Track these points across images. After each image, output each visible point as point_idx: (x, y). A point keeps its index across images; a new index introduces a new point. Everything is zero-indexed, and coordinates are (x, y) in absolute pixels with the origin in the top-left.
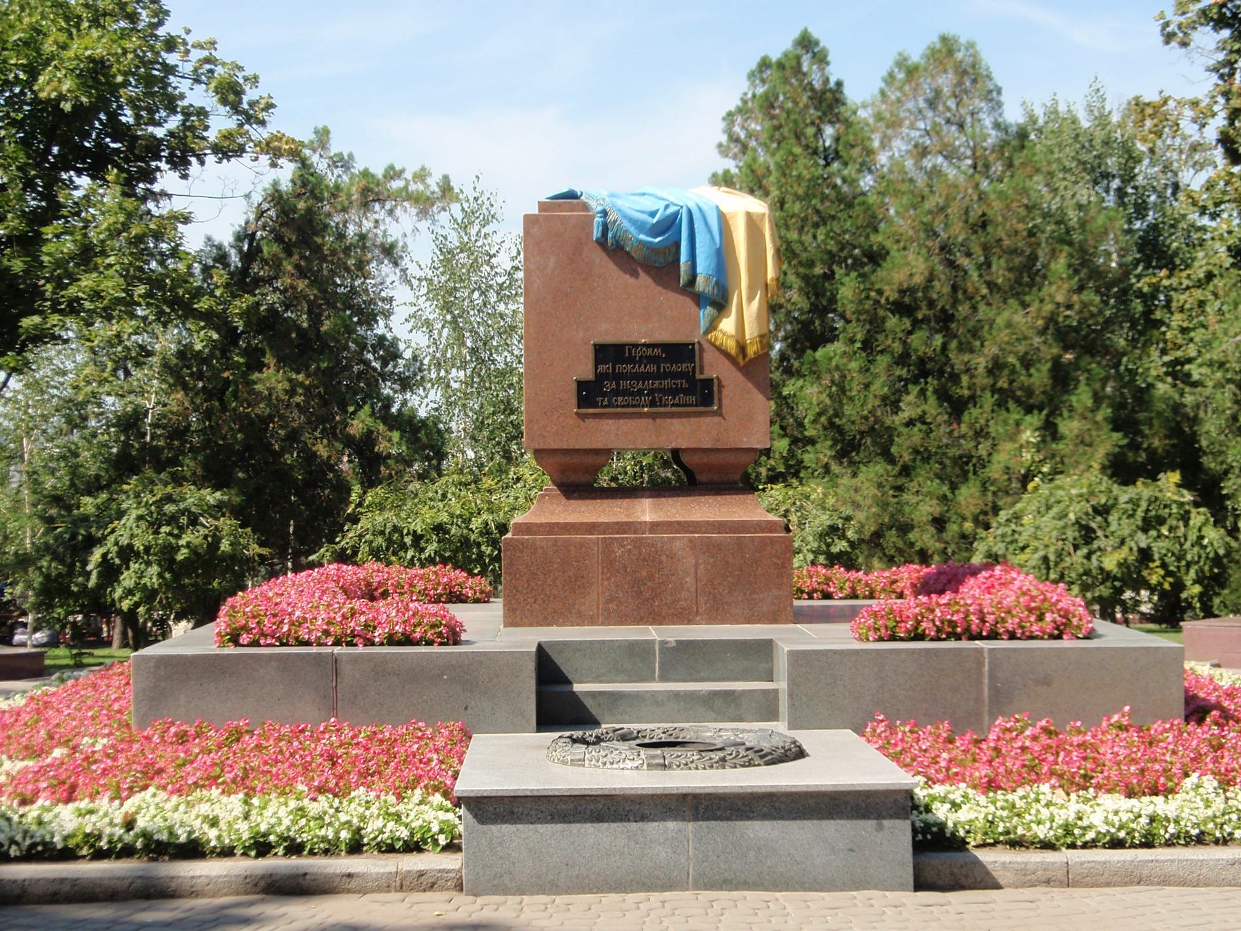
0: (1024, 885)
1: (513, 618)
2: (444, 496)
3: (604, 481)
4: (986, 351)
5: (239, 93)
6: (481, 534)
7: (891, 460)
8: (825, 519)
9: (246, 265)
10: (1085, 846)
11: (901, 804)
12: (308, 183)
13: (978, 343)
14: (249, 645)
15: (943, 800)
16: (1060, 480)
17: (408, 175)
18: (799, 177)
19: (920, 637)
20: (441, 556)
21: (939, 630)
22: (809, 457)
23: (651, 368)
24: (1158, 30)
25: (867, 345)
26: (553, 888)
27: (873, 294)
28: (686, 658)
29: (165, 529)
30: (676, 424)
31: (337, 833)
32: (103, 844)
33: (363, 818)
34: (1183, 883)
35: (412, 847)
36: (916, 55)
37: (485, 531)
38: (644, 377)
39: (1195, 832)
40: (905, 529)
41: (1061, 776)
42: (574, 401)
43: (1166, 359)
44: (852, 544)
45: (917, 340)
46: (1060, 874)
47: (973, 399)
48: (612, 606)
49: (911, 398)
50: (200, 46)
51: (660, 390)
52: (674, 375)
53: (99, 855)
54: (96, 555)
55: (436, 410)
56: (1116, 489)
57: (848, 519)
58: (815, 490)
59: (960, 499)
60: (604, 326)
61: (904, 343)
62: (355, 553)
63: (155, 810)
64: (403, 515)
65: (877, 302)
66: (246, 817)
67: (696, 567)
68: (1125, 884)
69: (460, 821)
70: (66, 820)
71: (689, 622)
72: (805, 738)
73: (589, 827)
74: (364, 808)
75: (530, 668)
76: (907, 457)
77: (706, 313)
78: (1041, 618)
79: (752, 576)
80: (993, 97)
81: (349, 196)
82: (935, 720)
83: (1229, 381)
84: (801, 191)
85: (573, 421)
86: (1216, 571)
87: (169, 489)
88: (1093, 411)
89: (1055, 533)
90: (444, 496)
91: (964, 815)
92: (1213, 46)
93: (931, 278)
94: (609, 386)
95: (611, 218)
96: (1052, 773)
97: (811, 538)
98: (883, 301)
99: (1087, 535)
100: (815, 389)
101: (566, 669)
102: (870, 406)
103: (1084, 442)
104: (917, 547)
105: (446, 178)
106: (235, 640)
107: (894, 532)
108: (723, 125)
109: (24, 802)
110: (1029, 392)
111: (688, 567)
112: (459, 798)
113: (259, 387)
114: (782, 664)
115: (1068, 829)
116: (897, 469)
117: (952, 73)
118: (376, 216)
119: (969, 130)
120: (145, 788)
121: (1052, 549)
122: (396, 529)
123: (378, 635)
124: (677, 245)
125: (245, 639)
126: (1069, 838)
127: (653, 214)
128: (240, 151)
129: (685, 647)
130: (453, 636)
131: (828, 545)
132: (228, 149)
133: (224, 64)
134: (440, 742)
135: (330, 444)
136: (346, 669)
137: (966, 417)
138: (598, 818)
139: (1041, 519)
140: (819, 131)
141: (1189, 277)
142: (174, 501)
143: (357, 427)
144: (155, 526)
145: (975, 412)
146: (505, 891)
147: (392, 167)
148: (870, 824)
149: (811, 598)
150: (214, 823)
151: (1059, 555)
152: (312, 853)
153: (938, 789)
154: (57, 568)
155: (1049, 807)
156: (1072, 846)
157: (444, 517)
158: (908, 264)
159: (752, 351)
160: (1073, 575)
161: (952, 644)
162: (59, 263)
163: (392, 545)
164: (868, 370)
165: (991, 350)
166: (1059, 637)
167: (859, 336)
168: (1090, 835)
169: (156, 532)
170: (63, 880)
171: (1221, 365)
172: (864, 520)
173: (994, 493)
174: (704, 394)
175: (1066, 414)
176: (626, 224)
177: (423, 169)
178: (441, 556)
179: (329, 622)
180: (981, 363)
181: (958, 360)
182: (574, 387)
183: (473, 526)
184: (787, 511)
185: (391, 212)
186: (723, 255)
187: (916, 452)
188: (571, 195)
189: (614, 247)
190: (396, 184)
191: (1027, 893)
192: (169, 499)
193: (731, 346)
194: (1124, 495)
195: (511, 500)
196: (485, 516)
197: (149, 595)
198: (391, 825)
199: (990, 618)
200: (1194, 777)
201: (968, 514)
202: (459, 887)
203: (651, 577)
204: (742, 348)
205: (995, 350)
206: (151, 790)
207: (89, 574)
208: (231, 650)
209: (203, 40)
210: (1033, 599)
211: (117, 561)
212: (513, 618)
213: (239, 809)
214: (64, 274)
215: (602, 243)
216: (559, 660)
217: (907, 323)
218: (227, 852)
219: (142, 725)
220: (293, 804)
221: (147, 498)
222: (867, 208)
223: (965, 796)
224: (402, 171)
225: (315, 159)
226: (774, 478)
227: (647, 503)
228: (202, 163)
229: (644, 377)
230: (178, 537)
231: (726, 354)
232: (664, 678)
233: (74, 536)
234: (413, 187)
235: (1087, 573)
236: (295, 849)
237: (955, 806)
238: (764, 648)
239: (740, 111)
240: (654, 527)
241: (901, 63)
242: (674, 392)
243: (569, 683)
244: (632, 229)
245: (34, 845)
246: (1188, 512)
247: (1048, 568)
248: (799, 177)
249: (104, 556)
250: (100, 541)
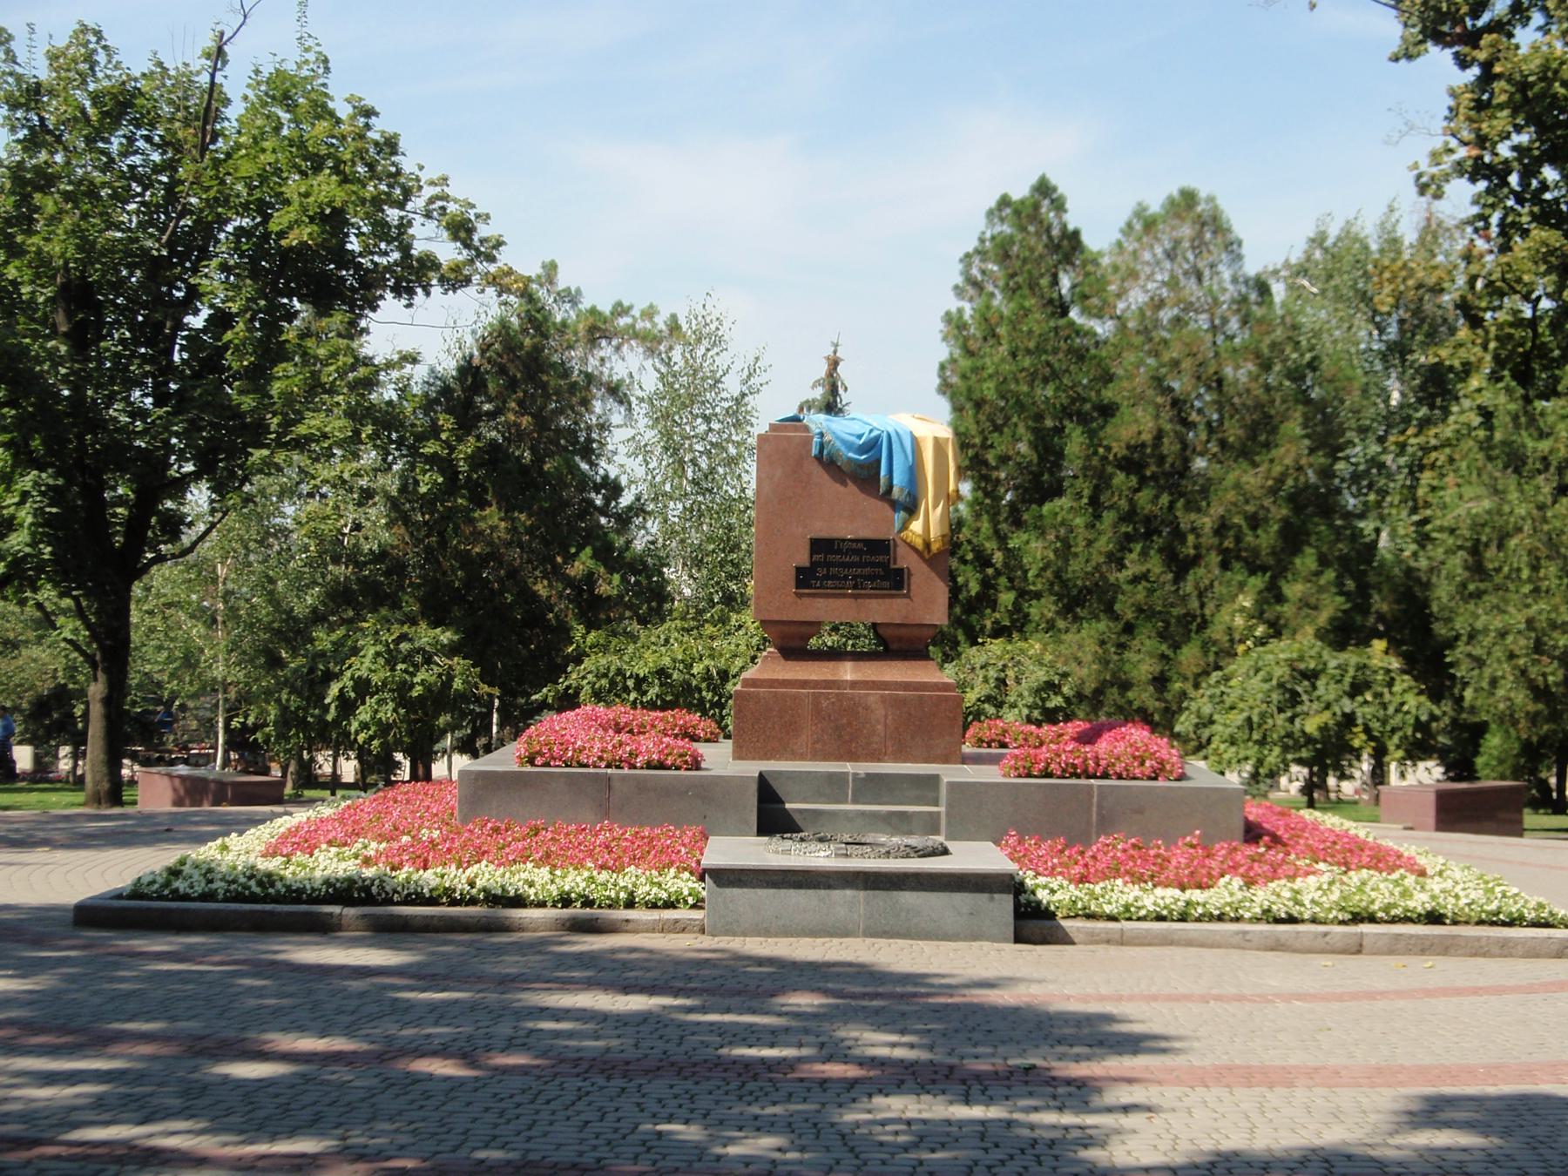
0: (1091, 943)
1: (739, 754)
2: (667, 641)
4: (1212, 511)
5: (470, 231)
6: (704, 679)
7: (1115, 617)
8: (1041, 675)
9: (462, 394)
10: (1139, 919)
12: (536, 319)
13: (1204, 504)
14: (543, 765)
15: (1045, 887)
16: (1274, 644)
17: (636, 312)
18: (1030, 332)
19: (1049, 775)
20: (663, 700)
21: (1064, 770)
22: (1034, 610)
23: (856, 559)
24: (1412, 181)
25: (1094, 501)
27: (1101, 450)
28: (874, 787)
29: (400, 666)
31: (618, 894)
32: (457, 895)
33: (634, 885)
34: (1202, 945)
35: (670, 905)
36: (1155, 206)
37: (707, 676)
39: (1216, 912)
40: (1125, 686)
41: (1132, 875)
42: (793, 583)
43: (1415, 518)
44: (1067, 700)
45: (1144, 497)
46: (1117, 937)
47: (1195, 561)
48: (818, 746)
49: (1134, 556)
50: (432, 183)
51: (861, 576)
52: (873, 565)
53: (454, 902)
54: (334, 689)
55: (653, 543)
56: (1326, 654)
57: (1065, 675)
58: (1032, 646)
59: (1182, 658)
61: (1131, 501)
62: (577, 694)
63: (487, 875)
64: (626, 658)
65: (1104, 458)
66: (552, 882)
67: (886, 717)
69: (704, 889)
70: (429, 878)
71: (879, 760)
72: (950, 845)
73: (792, 892)
74: (637, 879)
75: (754, 787)
76: (1130, 615)
77: (899, 516)
78: (1142, 764)
79: (943, 725)
80: (1232, 248)
81: (576, 333)
82: (1052, 835)
83: (1460, 548)
84: (1032, 345)
85: (792, 598)
86: (1419, 735)
87: (406, 628)
88: (1318, 574)
89: (1260, 696)
90: (667, 641)
91: (1058, 896)
92: (1468, 199)
93: (1159, 436)
94: (821, 572)
95: (826, 439)
96: (1127, 872)
97: (1026, 693)
98: (1111, 457)
99: (1294, 699)
100: (1040, 544)
101: (781, 793)
102: (1094, 563)
103: (1309, 605)
104: (1136, 705)
105: (674, 317)
106: (531, 761)
107: (1115, 690)
108: (960, 266)
109: (393, 869)
110: (1256, 552)
111: (879, 714)
112: (705, 871)
113: (482, 525)
115: (1127, 908)
116: (1120, 626)
117: (1194, 224)
118: (602, 354)
119: (1206, 283)
120: (479, 861)
121: (1256, 711)
122: (620, 672)
123: (639, 761)
124: (879, 461)
125: (539, 761)
126: (1128, 914)
127: (860, 437)
128: (467, 281)
129: (871, 777)
130: (696, 765)
131: (1043, 700)
132: (456, 280)
133: (456, 201)
134: (687, 841)
135: (550, 586)
136: (616, 784)
137: (1190, 578)
138: (798, 885)
139: (1249, 680)
140: (1055, 282)
141: (1436, 436)
142: (411, 640)
143: (577, 569)
144: (391, 663)
145: (1201, 571)
146: (734, 934)
147: (619, 304)
148: (986, 896)
149: (989, 746)
150: (531, 884)
151: (1263, 716)
152: (600, 907)
153: (1042, 880)
154: (294, 702)
155: (1119, 893)
156: (1130, 919)
157: (666, 661)
158: (1136, 421)
159: (935, 547)
160: (1275, 736)
161: (1074, 781)
162: (288, 397)
163: (613, 688)
164: (1093, 526)
165: (1217, 510)
166: (1155, 779)
167: (1086, 492)
168: (1143, 913)
169: (393, 669)
170: (433, 917)
171: (1452, 531)
172: (1085, 674)
173: (1216, 653)
174: (896, 581)
175: (1290, 577)
176: (838, 444)
177: (651, 306)
178: (663, 700)
179: (603, 750)
180: (1207, 522)
181: (1185, 519)
182: (794, 572)
183: (695, 671)
184: (1005, 666)
185: (618, 348)
186: (915, 471)
187: (1140, 610)
189: (829, 463)
190: (623, 322)
191: (1092, 947)
192: (403, 637)
193: (919, 543)
194: (1333, 660)
195: (733, 647)
196: (707, 662)
197: (384, 729)
198: (655, 890)
199: (1103, 763)
200: (1227, 877)
201: (1189, 674)
202: (702, 931)
203: (850, 724)
204: (927, 545)
205: (1221, 511)
206: (484, 862)
207: (326, 709)
208: (529, 768)
209: (435, 177)
210: (1137, 749)
211: (353, 695)
212: (739, 754)
213: (548, 877)
214: (293, 411)
215: (819, 458)
216: (775, 785)
217: (1134, 481)
218: (542, 904)
219: (465, 821)
220: (586, 874)
221: (385, 636)
222: (1100, 362)
223: (1061, 886)
224: (630, 308)
225: (542, 293)
226: (999, 632)
227: (849, 665)
228: (428, 294)
230: (413, 675)
231: (914, 548)
232: (855, 801)
233: (312, 670)
234: (640, 325)
235: (1289, 735)
236: (588, 903)
237: (1053, 892)
238: (934, 780)
239: (977, 252)
240: (854, 684)
241: (1140, 212)
242: (872, 578)
245: (409, 895)
246: (1393, 679)
247: (1251, 729)
248: (1030, 332)
249: (341, 690)
250: (337, 676)
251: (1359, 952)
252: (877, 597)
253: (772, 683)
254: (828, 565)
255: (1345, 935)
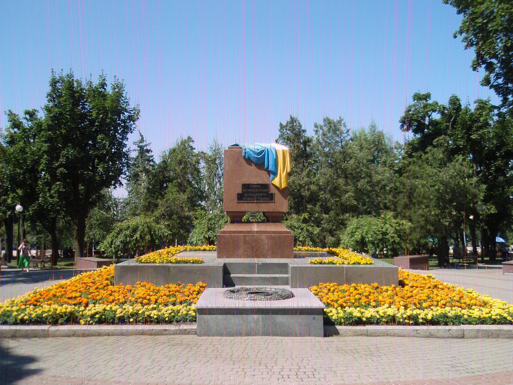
0: (354, 336)
1: (219, 257)
3: (243, 220)
11: (321, 312)
26: (222, 335)
28: (264, 268)
30: (263, 205)
34: (399, 336)
38: (255, 193)
42: (236, 199)
48: (246, 253)
52: (263, 192)
60: (245, 179)
67: (268, 243)
68: (384, 336)
72: (294, 291)
114: (290, 270)
129: (264, 265)
136: (171, 270)
174: (271, 197)
182: (237, 195)
188: (237, 145)
189: (249, 161)
191: (355, 338)
202: (196, 334)
215: (244, 157)
229: (255, 193)
232: (258, 273)
238: (286, 265)
240: (257, 232)
242: (263, 197)
243: (230, 274)
244: (252, 153)
251: (463, 337)
252: (264, 203)
253: (230, 232)
254: (248, 193)
255: (457, 330)
